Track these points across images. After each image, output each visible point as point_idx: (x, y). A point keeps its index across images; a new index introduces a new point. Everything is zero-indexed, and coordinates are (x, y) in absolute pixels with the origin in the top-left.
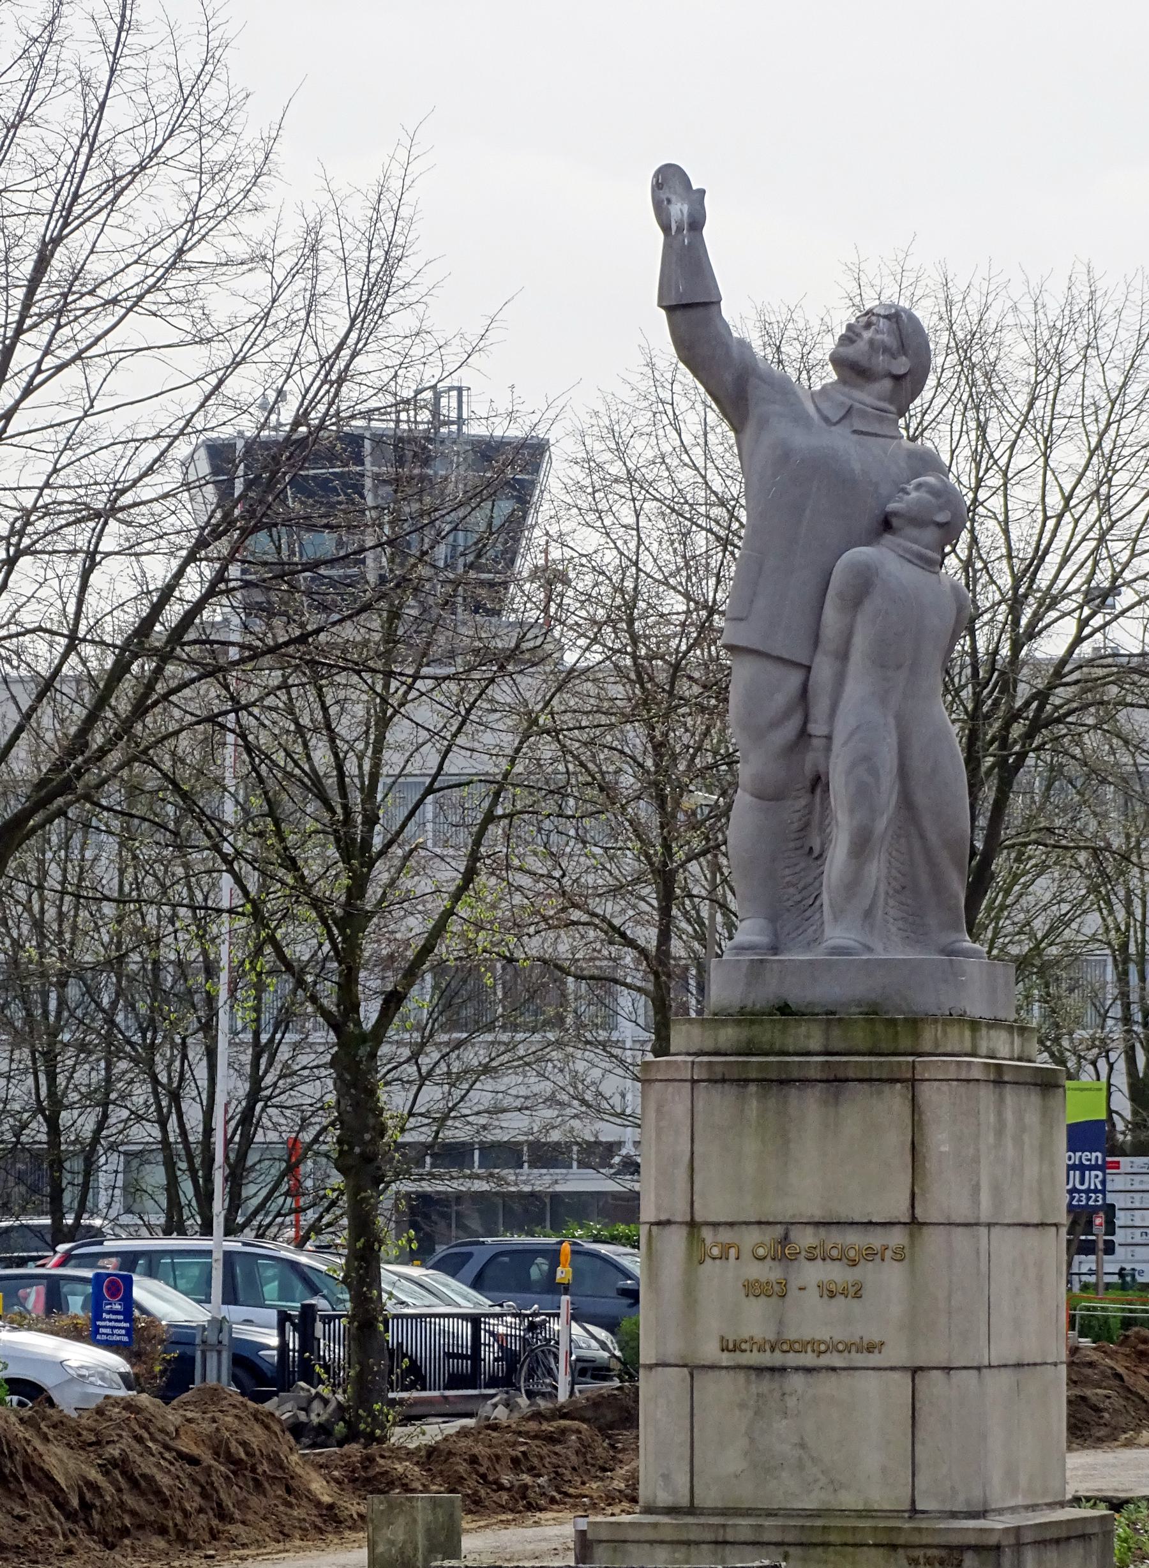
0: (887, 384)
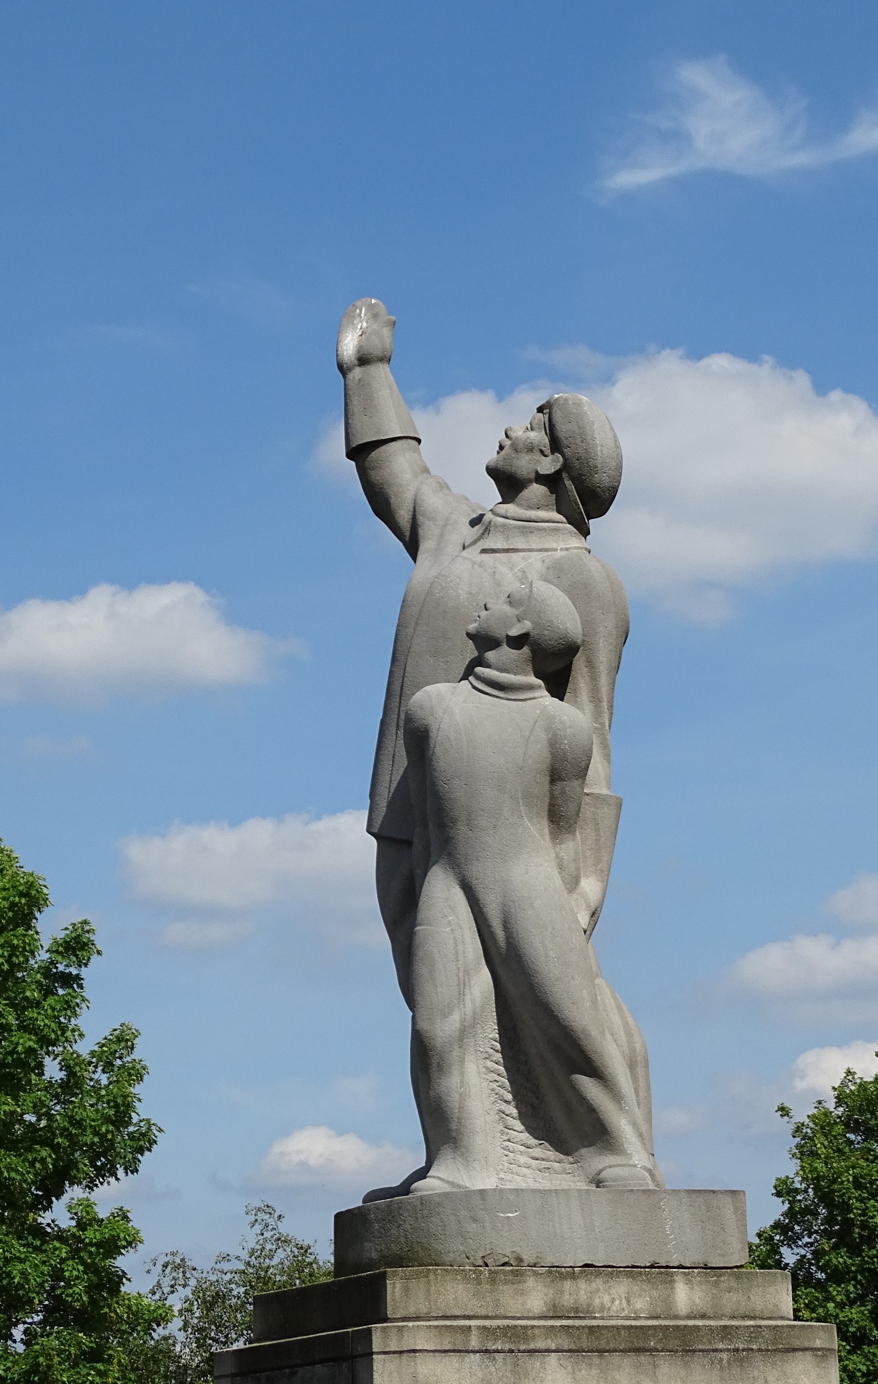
0: (537, 490)
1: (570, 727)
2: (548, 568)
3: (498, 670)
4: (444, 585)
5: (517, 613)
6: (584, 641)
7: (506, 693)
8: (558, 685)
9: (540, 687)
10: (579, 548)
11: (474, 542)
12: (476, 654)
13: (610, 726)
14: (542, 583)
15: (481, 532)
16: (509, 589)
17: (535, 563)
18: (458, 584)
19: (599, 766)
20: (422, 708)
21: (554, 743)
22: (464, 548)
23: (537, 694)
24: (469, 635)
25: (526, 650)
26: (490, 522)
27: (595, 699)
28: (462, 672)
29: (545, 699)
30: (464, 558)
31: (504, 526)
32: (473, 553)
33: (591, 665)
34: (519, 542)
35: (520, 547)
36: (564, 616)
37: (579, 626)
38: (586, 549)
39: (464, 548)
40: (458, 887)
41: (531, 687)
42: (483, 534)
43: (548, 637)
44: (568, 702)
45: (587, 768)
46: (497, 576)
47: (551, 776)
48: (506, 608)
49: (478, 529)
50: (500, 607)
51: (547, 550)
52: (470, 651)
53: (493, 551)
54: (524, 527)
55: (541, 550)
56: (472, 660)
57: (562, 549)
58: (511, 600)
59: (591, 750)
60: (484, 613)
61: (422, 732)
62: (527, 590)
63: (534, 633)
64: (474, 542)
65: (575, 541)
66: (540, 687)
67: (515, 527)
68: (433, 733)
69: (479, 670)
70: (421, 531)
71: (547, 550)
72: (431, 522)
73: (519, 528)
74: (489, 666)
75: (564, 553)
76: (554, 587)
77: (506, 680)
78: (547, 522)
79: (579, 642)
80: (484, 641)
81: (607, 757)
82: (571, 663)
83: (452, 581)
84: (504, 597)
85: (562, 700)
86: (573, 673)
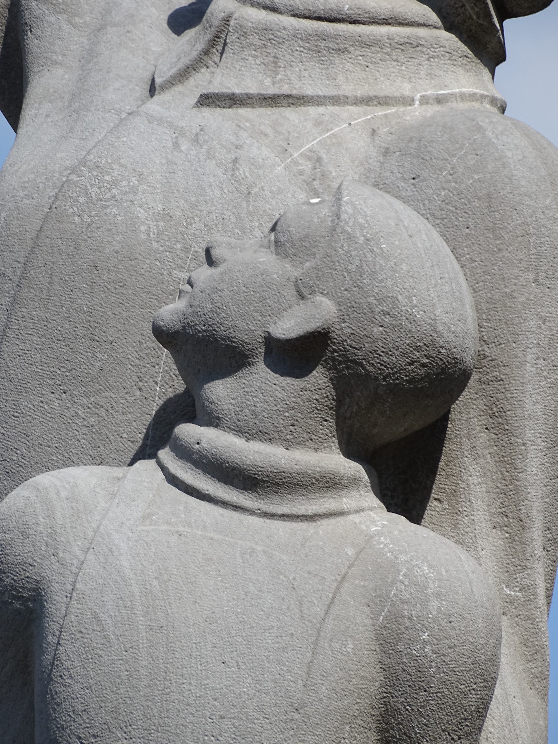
1: (438, 596)
2: (386, 152)
3: (240, 431)
4: (94, 191)
5: (295, 273)
6: (481, 356)
7: (260, 497)
8: (406, 475)
9: (355, 482)
10: (472, 97)
11: (183, 75)
12: (179, 386)
13: (549, 597)
14: (367, 191)
15: (200, 46)
16: (275, 207)
17: (344, 137)
18: (134, 191)
19: (517, 705)
20: (25, 535)
21: (391, 640)
22: (152, 90)
23: (346, 501)
24: (163, 335)
25: (319, 378)
26: (226, 21)
27: (510, 517)
28: (140, 437)
29: (366, 515)
30: (151, 119)
31: (265, 30)
32: (177, 104)
33: (499, 421)
34: (306, 78)
35: (309, 91)
36: (427, 289)
37: (470, 314)
38: (493, 101)
39: (152, 90)
40: (372, 495)
41: (330, 483)
42: (207, 52)
43: (381, 344)
44: (435, 527)
45: (482, 711)
46: (243, 170)
47: (381, 731)
48: (267, 259)
49: (193, 39)
50: (249, 256)
51: (384, 101)
52: (164, 378)
53: (233, 100)
54: (324, 37)
55: (367, 101)
56: (170, 401)
57: (425, 100)
58: (279, 237)
59: (494, 660)
60: (203, 274)
61: (24, 600)
62: (325, 211)
63: (342, 333)
64: (183, 75)
65: (461, 79)
66: (355, 482)
67: (296, 35)
68: (56, 604)
69: (187, 431)
70: (34, 44)
71: (384, 101)
72: (62, 18)
73: (307, 37)
74: (213, 421)
75: (432, 110)
76: (400, 206)
77: (259, 461)
78: (386, 22)
79: (469, 359)
80: (203, 352)
81: (540, 681)
82: (445, 418)
83: (114, 183)
84: (260, 231)
85: (415, 515)
86: (448, 446)
